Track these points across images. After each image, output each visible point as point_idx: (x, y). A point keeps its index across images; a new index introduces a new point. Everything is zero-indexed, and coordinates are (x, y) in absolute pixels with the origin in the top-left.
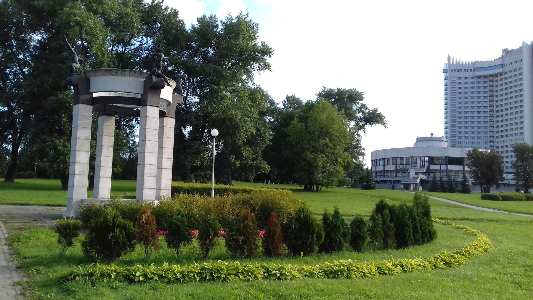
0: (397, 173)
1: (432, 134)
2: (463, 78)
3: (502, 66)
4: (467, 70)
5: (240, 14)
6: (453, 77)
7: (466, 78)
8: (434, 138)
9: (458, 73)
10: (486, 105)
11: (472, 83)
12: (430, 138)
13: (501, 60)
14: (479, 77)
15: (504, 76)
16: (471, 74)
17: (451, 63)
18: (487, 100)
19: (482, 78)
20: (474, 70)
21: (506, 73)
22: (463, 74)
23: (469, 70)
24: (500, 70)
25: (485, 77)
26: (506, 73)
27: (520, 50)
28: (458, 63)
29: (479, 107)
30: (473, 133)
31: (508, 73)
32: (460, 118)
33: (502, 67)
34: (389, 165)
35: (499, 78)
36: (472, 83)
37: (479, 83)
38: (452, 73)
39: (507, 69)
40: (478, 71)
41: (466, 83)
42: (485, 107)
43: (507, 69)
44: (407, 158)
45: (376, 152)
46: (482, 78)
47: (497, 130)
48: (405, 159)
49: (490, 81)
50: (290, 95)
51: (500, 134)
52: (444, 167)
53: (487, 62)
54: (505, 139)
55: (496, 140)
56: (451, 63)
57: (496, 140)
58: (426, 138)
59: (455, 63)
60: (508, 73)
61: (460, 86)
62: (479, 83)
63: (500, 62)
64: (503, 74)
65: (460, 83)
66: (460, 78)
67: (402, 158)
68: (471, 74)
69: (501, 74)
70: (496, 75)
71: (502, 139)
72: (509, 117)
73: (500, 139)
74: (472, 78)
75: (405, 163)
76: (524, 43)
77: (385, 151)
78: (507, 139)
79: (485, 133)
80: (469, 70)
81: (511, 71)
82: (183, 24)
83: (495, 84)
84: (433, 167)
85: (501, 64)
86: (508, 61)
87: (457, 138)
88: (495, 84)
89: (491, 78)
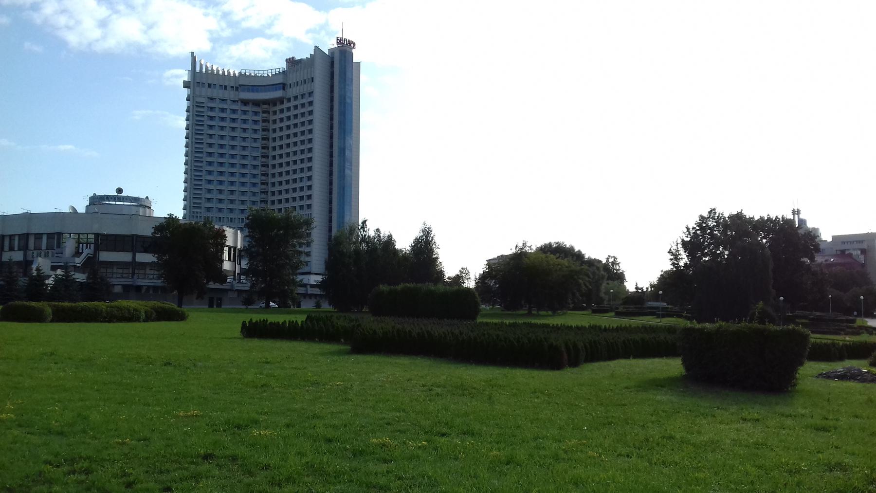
1: (120, 191)
3: (283, 86)
4: (226, 87)
5: (462, 272)
6: (200, 96)
9: (209, 90)
13: (281, 76)
14: (245, 102)
15: (286, 105)
17: (198, 69)
18: (258, 145)
19: (251, 105)
20: (237, 89)
21: (289, 100)
22: (218, 93)
24: (278, 94)
25: (256, 103)
26: (289, 100)
27: (309, 63)
28: (210, 73)
31: (292, 99)
33: (284, 89)
34: (11, 249)
35: (278, 107)
37: (245, 112)
38: (197, 89)
40: (243, 91)
42: (255, 158)
44: (50, 236)
46: (251, 105)
47: (273, 198)
48: (45, 238)
49: (264, 112)
52: (124, 257)
59: (204, 71)
60: (292, 99)
62: (245, 112)
63: (280, 80)
64: (285, 101)
67: (38, 236)
68: (230, 95)
70: (274, 102)
72: (292, 177)
75: (44, 247)
77: (28, 217)
81: (296, 98)
82: (389, 242)
84: (105, 256)
86: (292, 79)
87: (203, 210)
89: (265, 106)
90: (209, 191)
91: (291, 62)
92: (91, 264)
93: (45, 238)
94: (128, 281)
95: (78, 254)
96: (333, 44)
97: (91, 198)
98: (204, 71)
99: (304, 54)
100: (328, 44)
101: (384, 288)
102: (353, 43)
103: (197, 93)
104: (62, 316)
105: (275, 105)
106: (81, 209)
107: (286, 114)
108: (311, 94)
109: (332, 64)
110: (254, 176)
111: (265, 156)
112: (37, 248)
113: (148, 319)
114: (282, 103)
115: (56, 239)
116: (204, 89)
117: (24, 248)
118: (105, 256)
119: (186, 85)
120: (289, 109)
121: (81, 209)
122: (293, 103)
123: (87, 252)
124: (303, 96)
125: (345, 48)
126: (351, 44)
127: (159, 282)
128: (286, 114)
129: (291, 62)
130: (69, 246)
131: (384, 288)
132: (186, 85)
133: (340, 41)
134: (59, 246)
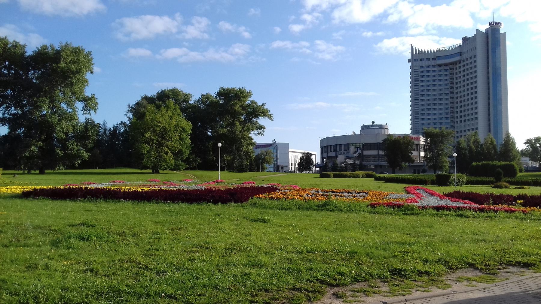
0: (379, 158)
1: (373, 122)
2: (425, 67)
3: (460, 54)
4: (429, 59)
6: (416, 66)
7: (428, 67)
8: (376, 125)
9: (421, 62)
10: (447, 92)
11: (434, 71)
12: (371, 126)
14: (440, 66)
15: (462, 64)
16: (432, 63)
17: (414, 52)
18: (448, 87)
23: (431, 59)
25: (446, 65)
27: (474, 38)
28: (421, 53)
29: (440, 95)
30: (429, 119)
32: (423, 105)
33: (461, 55)
34: (331, 151)
35: (458, 66)
36: (434, 71)
37: (440, 71)
39: (464, 57)
40: (439, 59)
41: (428, 71)
42: (447, 94)
43: (464, 57)
45: (328, 139)
48: (343, 146)
49: (450, 69)
50: (205, 94)
51: (459, 119)
52: (374, 152)
53: (445, 50)
54: (463, 124)
55: (456, 125)
56: (414, 52)
57: (456, 125)
58: (368, 126)
59: (418, 52)
61: (423, 74)
64: (461, 62)
65: (422, 72)
66: (422, 67)
67: (340, 145)
68: (432, 63)
69: (459, 62)
70: (456, 63)
71: (472, 122)
73: (459, 124)
74: (434, 66)
76: (477, 31)
78: (469, 123)
79: (447, 118)
80: (431, 59)
81: (467, 59)
83: (455, 71)
84: (366, 153)
85: (458, 52)
88: (455, 71)
89: (451, 66)
90: (423, 114)
91: (465, 39)
92: (361, 157)
93: (343, 146)
94: (376, 163)
95: (355, 152)
96: (487, 26)
97: (362, 127)
98: (418, 52)
99: (471, 34)
100: (483, 28)
101: (474, 164)
102: (499, 23)
103: (415, 65)
104: (336, 176)
105: (456, 64)
106: (358, 133)
107: (462, 69)
108: (475, 56)
109: (487, 37)
110: (447, 104)
111: (452, 93)
112: (340, 150)
113: (363, 177)
114: (460, 63)
115: (347, 146)
116: (418, 62)
117: (335, 150)
118: (366, 153)
119: (409, 61)
120: (464, 66)
121: (358, 133)
122: (466, 62)
123: (359, 151)
124: (471, 58)
125: (494, 27)
126: (499, 24)
127: (385, 163)
128: (462, 69)
129: (465, 39)
130: (352, 149)
131: (474, 164)
132: (409, 61)
133: (491, 24)
134: (348, 149)
